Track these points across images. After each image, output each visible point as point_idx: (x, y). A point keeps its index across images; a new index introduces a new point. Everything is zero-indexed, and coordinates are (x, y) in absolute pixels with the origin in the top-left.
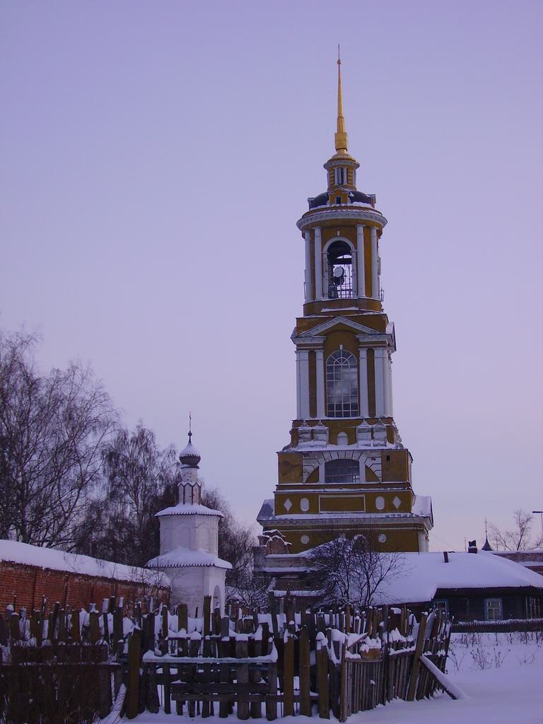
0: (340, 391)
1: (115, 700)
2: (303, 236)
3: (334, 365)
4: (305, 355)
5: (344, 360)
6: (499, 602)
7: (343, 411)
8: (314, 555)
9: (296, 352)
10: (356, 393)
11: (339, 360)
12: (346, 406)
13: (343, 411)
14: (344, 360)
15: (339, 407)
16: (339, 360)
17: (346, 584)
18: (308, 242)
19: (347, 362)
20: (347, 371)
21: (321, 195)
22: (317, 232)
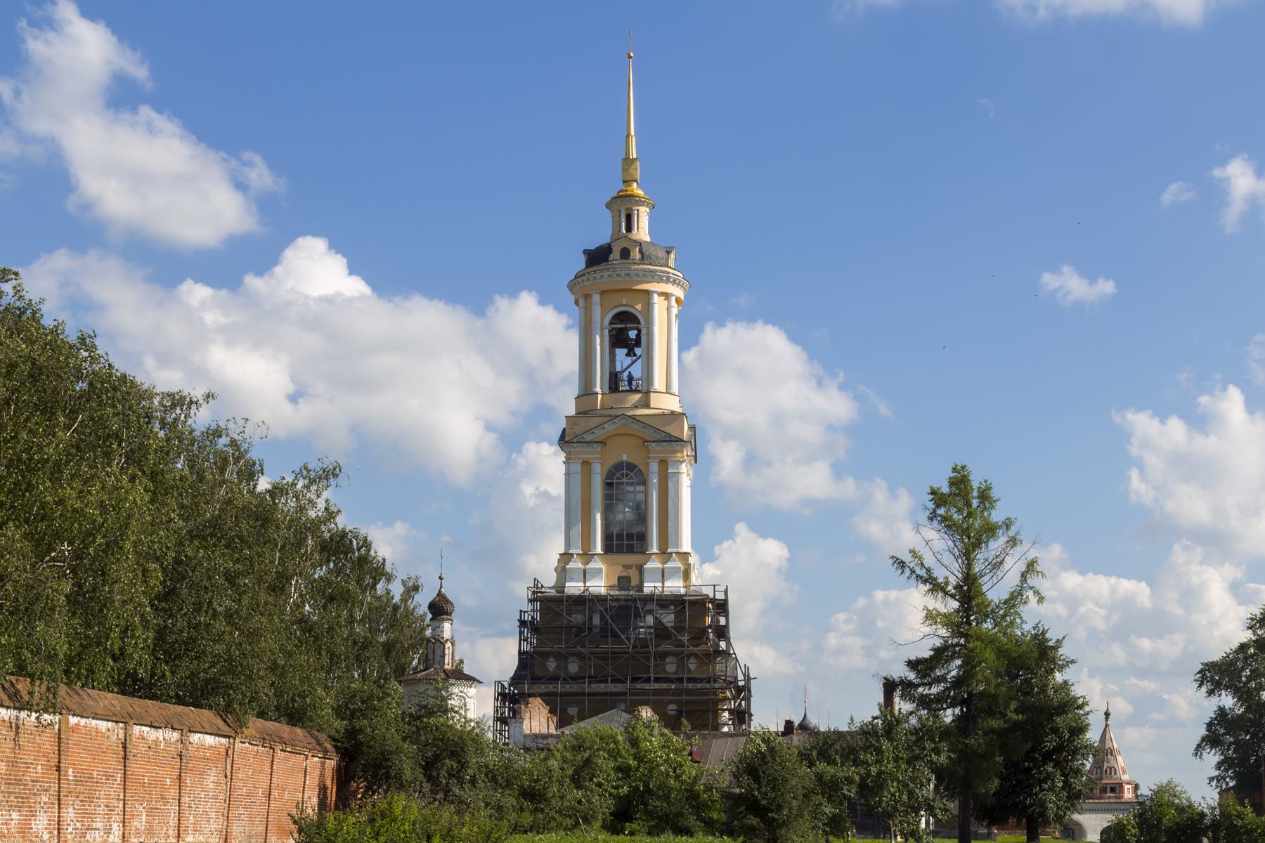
0: (625, 513)
1: (334, 768)
2: (577, 303)
3: (625, 472)
4: (577, 467)
5: (627, 475)
6: (727, 712)
7: (625, 543)
8: (963, 724)
9: (564, 463)
10: (642, 518)
11: (622, 475)
12: (630, 536)
13: (625, 543)
14: (627, 475)
15: (620, 537)
16: (622, 475)
17: (229, 777)
18: (583, 310)
19: (632, 477)
20: (631, 489)
21: (598, 247)
22: (596, 298)
